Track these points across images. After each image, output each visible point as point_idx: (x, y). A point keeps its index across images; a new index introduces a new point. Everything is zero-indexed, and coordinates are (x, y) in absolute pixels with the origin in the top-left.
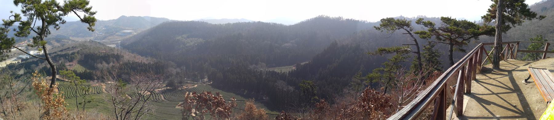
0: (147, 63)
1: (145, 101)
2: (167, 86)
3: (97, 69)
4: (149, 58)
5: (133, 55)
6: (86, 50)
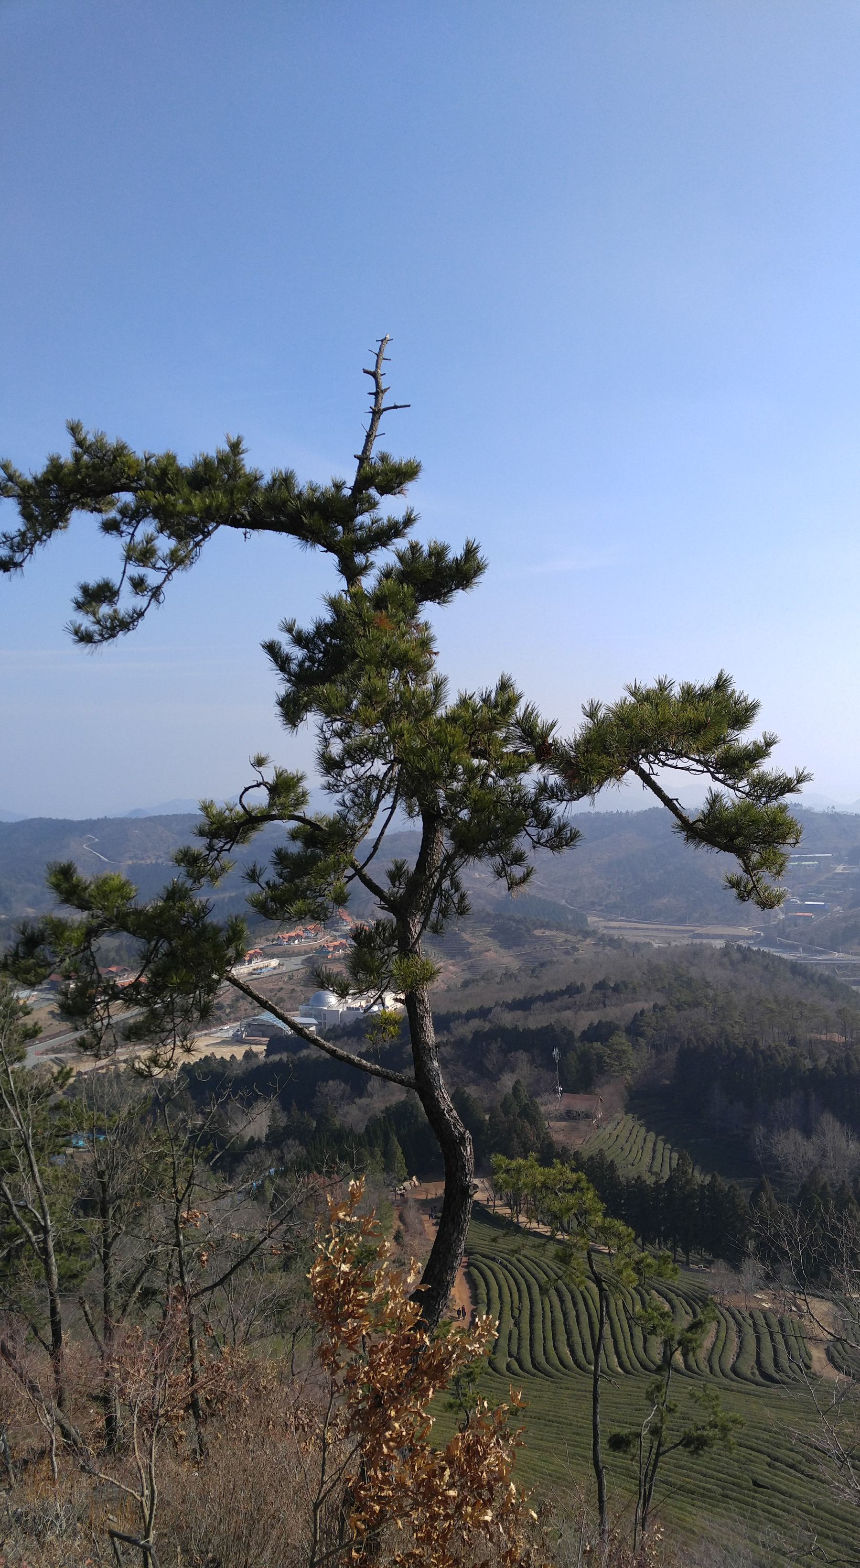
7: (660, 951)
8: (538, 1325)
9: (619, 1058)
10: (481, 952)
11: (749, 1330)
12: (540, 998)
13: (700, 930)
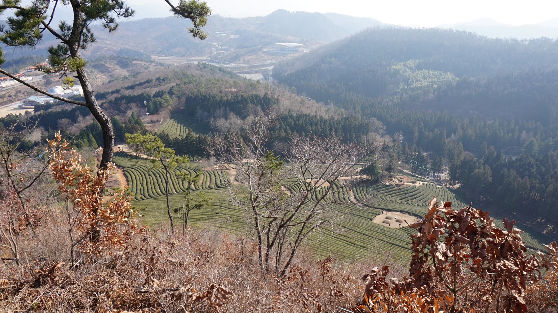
0: (326, 117)
1: (319, 201)
2: (361, 173)
3: (216, 130)
4: (332, 107)
5: (299, 99)
6: (191, 86)
7: (177, 66)
8: (149, 185)
9: (166, 102)
10: (114, 70)
11: (213, 176)
12: (137, 85)
13: (190, 59)
